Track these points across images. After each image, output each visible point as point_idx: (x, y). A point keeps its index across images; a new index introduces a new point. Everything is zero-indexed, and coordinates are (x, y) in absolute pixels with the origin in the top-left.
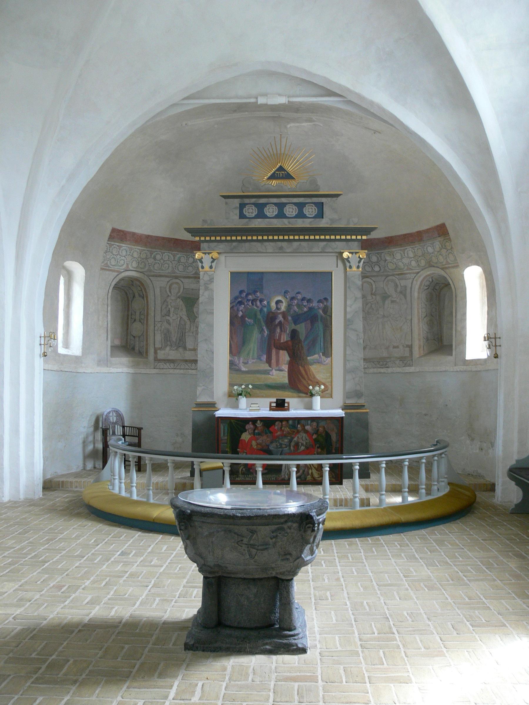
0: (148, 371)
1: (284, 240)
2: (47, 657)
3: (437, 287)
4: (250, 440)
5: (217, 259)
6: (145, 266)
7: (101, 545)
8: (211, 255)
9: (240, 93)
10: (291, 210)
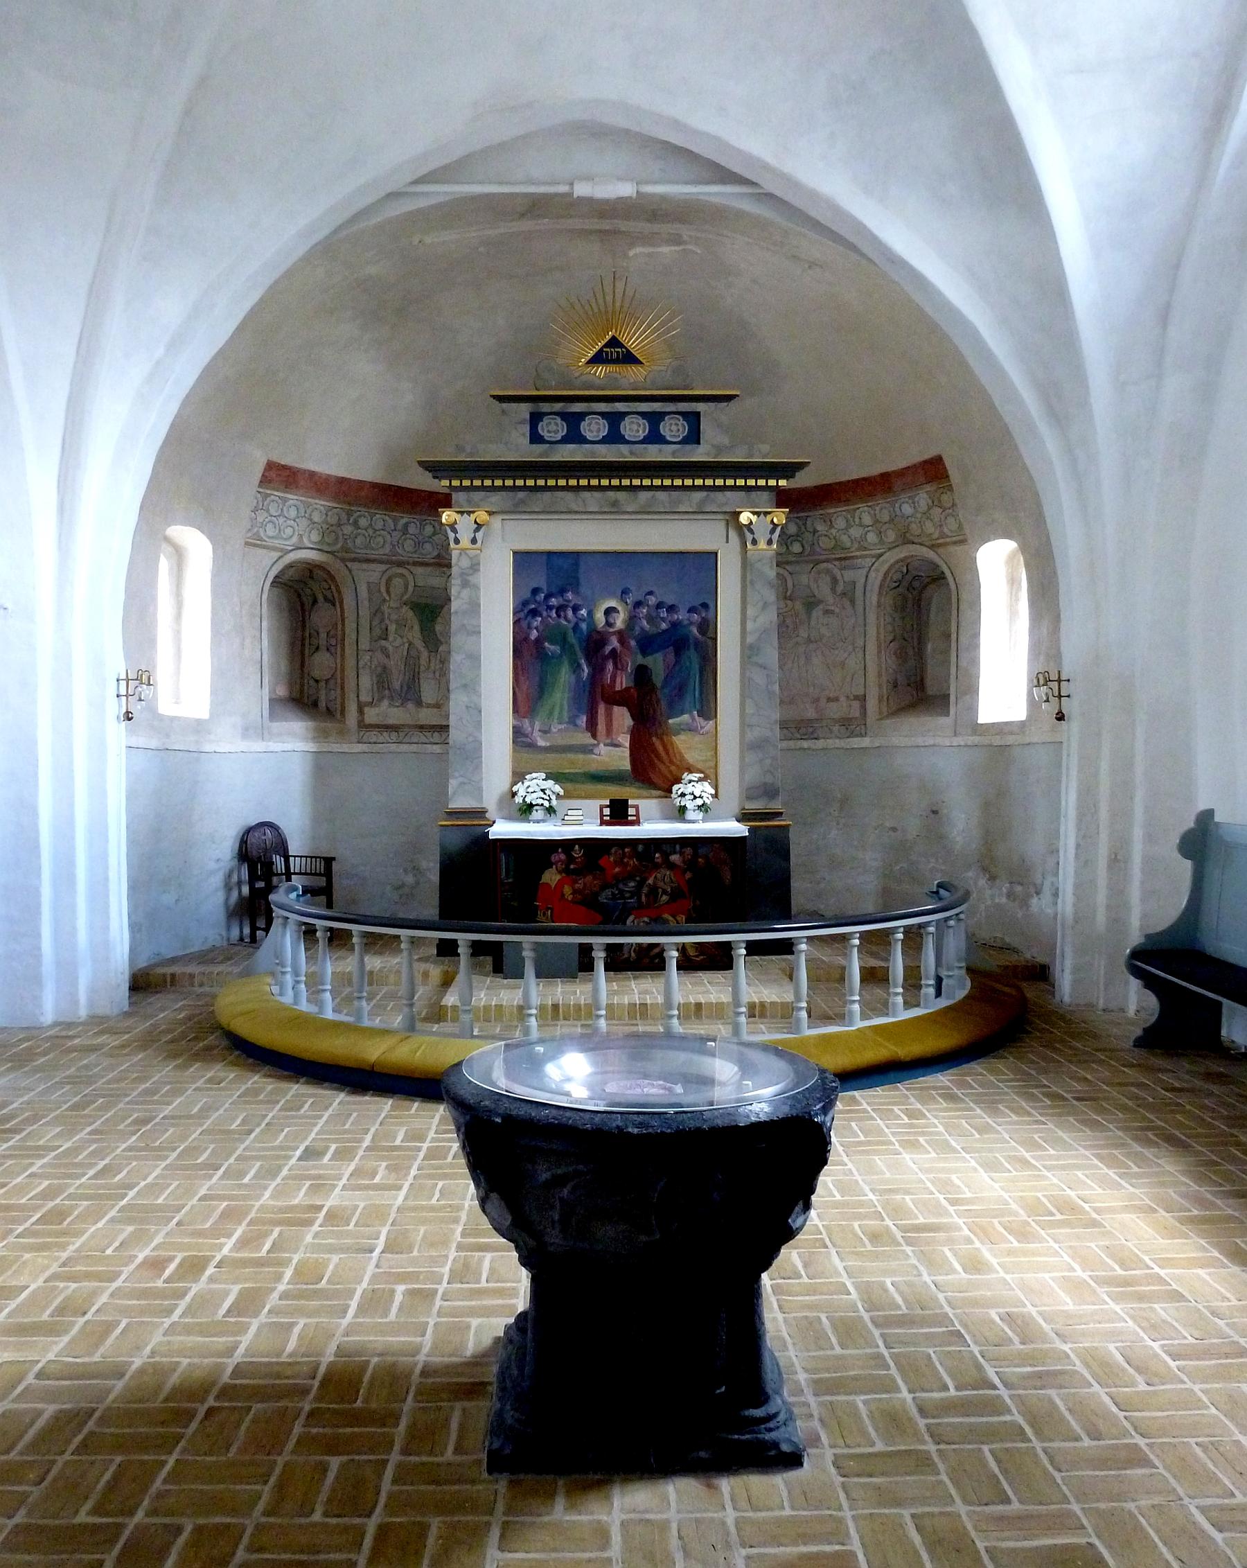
0: (345, 748)
1: (620, 488)
2: (119, 1520)
3: (916, 584)
4: (560, 884)
5: (487, 524)
6: (337, 539)
7: (258, 1130)
8: (473, 517)
9: (537, 174)
10: (635, 427)
